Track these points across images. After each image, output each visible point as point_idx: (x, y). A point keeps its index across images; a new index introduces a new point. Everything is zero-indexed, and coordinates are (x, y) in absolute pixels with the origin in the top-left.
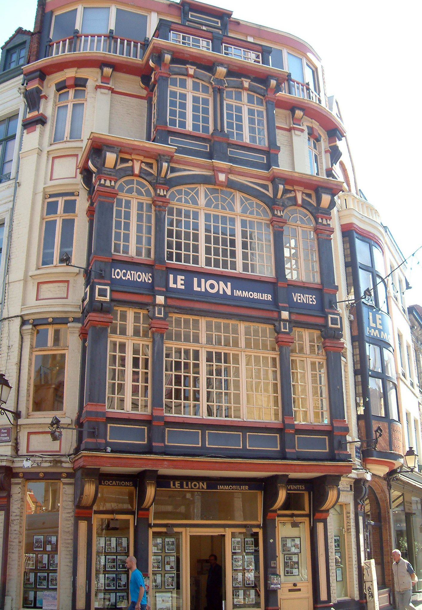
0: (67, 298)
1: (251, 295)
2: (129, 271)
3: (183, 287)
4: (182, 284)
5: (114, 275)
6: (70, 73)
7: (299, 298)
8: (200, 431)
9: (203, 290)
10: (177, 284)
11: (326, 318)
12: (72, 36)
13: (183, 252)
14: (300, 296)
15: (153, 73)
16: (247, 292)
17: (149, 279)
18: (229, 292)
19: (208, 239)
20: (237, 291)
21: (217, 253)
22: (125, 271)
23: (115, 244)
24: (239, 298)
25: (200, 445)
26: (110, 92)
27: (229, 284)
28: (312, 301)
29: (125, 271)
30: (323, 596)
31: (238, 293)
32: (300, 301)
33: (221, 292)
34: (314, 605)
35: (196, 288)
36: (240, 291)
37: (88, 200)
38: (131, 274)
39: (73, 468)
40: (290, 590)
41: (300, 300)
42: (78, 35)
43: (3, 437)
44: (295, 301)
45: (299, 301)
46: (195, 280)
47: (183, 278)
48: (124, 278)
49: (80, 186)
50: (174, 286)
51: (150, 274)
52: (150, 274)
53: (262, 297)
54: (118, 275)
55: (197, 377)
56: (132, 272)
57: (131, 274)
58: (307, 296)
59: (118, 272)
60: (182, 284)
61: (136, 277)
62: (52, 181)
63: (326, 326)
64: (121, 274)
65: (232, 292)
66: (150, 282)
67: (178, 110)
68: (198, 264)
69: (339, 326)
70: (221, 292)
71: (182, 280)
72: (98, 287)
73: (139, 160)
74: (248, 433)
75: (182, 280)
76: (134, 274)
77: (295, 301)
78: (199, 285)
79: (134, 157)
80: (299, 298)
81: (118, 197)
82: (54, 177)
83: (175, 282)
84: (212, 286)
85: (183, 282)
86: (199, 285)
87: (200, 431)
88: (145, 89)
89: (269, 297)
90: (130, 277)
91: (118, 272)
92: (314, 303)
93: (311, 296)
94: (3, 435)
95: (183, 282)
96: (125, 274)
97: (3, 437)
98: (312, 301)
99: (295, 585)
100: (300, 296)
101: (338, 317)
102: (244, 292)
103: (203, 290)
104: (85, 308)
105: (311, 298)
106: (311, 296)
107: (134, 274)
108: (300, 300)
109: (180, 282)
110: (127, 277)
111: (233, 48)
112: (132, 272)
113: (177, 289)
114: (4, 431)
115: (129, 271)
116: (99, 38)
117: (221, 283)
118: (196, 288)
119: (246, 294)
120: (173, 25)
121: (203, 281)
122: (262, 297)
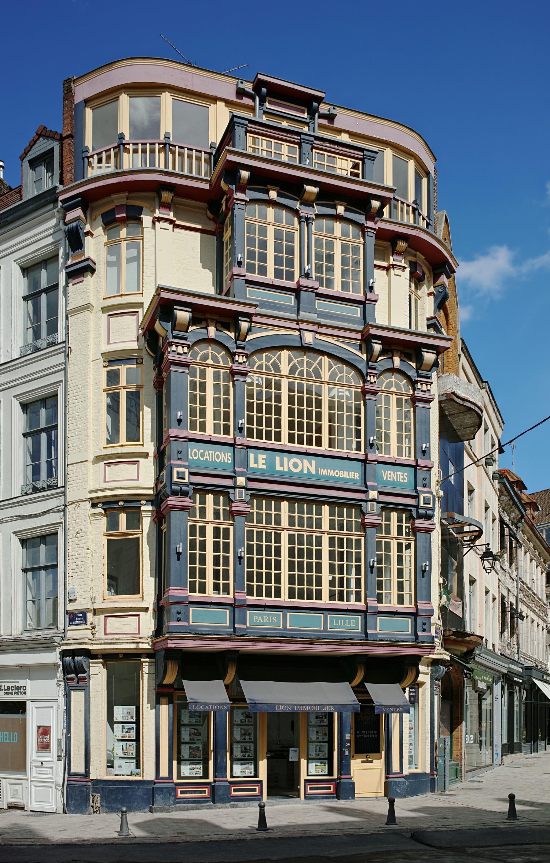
0: (138, 479)
1: (337, 473)
2: (207, 451)
3: (264, 467)
4: (263, 464)
5: (191, 456)
6: (120, 199)
7: (402, 477)
9: (286, 470)
10: (258, 464)
12: (116, 144)
13: (264, 428)
14: (390, 474)
15: (225, 197)
16: (332, 471)
17: (228, 459)
18: (313, 472)
19: (291, 400)
20: (322, 469)
21: (301, 428)
22: (202, 451)
23: (191, 421)
24: (324, 477)
25: (281, 627)
27: (314, 462)
28: (404, 479)
29: (202, 451)
31: (323, 472)
32: (390, 480)
33: (305, 471)
35: (279, 468)
36: (326, 470)
37: (154, 369)
38: (209, 454)
39: (153, 649)
41: (390, 478)
42: (124, 142)
43: (78, 620)
44: (385, 479)
45: (389, 479)
46: (278, 459)
47: (264, 456)
48: (202, 459)
49: (144, 352)
50: (255, 466)
51: (230, 454)
52: (230, 454)
53: (349, 475)
54: (195, 454)
56: (210, 452)
57: (209, 454)
58: (398, 473)
59: (195, 452)
60: (263, 464)
61: (215, 457)
62: (110, 345)
64: (199, 455)
65: (317, 470)
66: (229, 462)
67: (256, 263)
68: (266, 276)
69: (431, 506)
70: (305, 471)
71: (263, 459)
72: (175, 470)
73: (214, 319)
75: (263, 459)
76: (212, 454)
77: (385, 479)
78: (282, 465)
79: (207, 316)
80: (402, 477)
82: (111, 342)
83: (256, 462)
84: (296, 465)
85: (264, 461)
86: (282, 465)
88: (213, 220)
89: (173, 487)
90: (208, 457)
91: (195, 452)
92: (406, 481)
93: (402, 473)
94: (79, 619)
95: (264, 461)
96: (203, 455)
97: (78, 620)
98: (404, 479)
101: (431, 496)
102: (329, 470)
103: (286, 470)
104: (160, 491)
105: (402, 475)
106: (402, 473)
107: (212, 454)
108: (390, 478)
109: (261, 461)
110: (205, 457)
111: (326, 156)
112: (210, 452)
113: (258, 469)
114: (79, 615)
115: (207, 451)
116: (152, 146)
118: (279, 468)
119: (331, 473)
121: (286, 459)
122: (349, 475)
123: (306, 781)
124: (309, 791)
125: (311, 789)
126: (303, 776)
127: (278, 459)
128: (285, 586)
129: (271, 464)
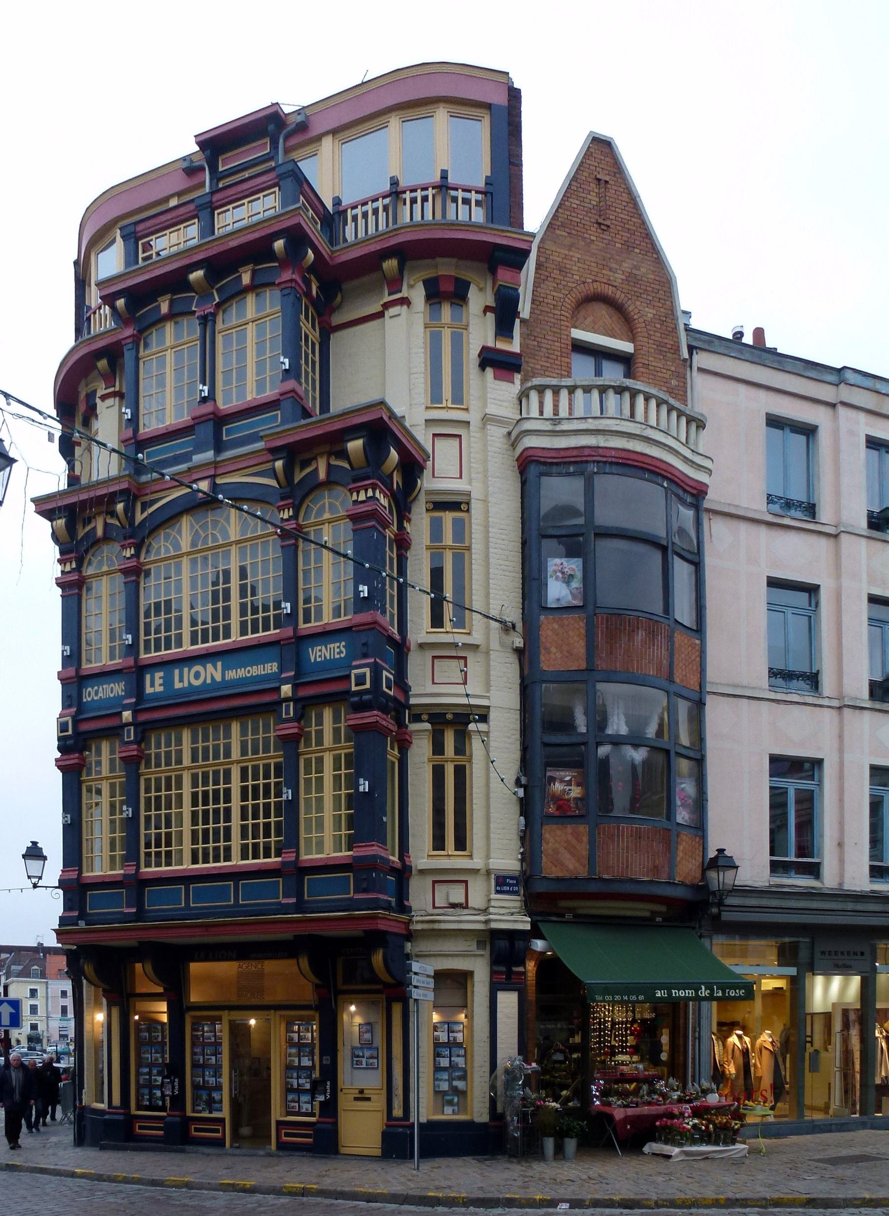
7: (319, 654)
8: (183, 887)
11: (348, 677)
18: (218, 678)
26: (117, 399)
27: (219, 664)
28: (340, 652)
30: (398, 1112)
31: (231, 675)
34: (335, 1124)
40: (356, 1099)
45: (319, 659)
47: (161, 674)
55: (242, 820)
58: (332, 646)
60: (160, 685)
63: (348, 693)
64: (93, 694)
65: (223, 675)
70: (209, 681)
74: (306, 898)
80: (319, 654)
81: (144, 568)
86: (181, 680)
87: (183, 887)
96: (96, 693)
99: (361, 1091)
100: (320, 651)
105: (338, 647)
108: (320, 656)
110: (100, 695)
117: (209, 666)
119: (241, 673)
120: (140, 227)
123: (279, 1123)
124: (284, 1138)
125: (287, 1135)
126: (277, 1113)
127: (177, 672)
128: (236, 842)
129: (168, 682)
